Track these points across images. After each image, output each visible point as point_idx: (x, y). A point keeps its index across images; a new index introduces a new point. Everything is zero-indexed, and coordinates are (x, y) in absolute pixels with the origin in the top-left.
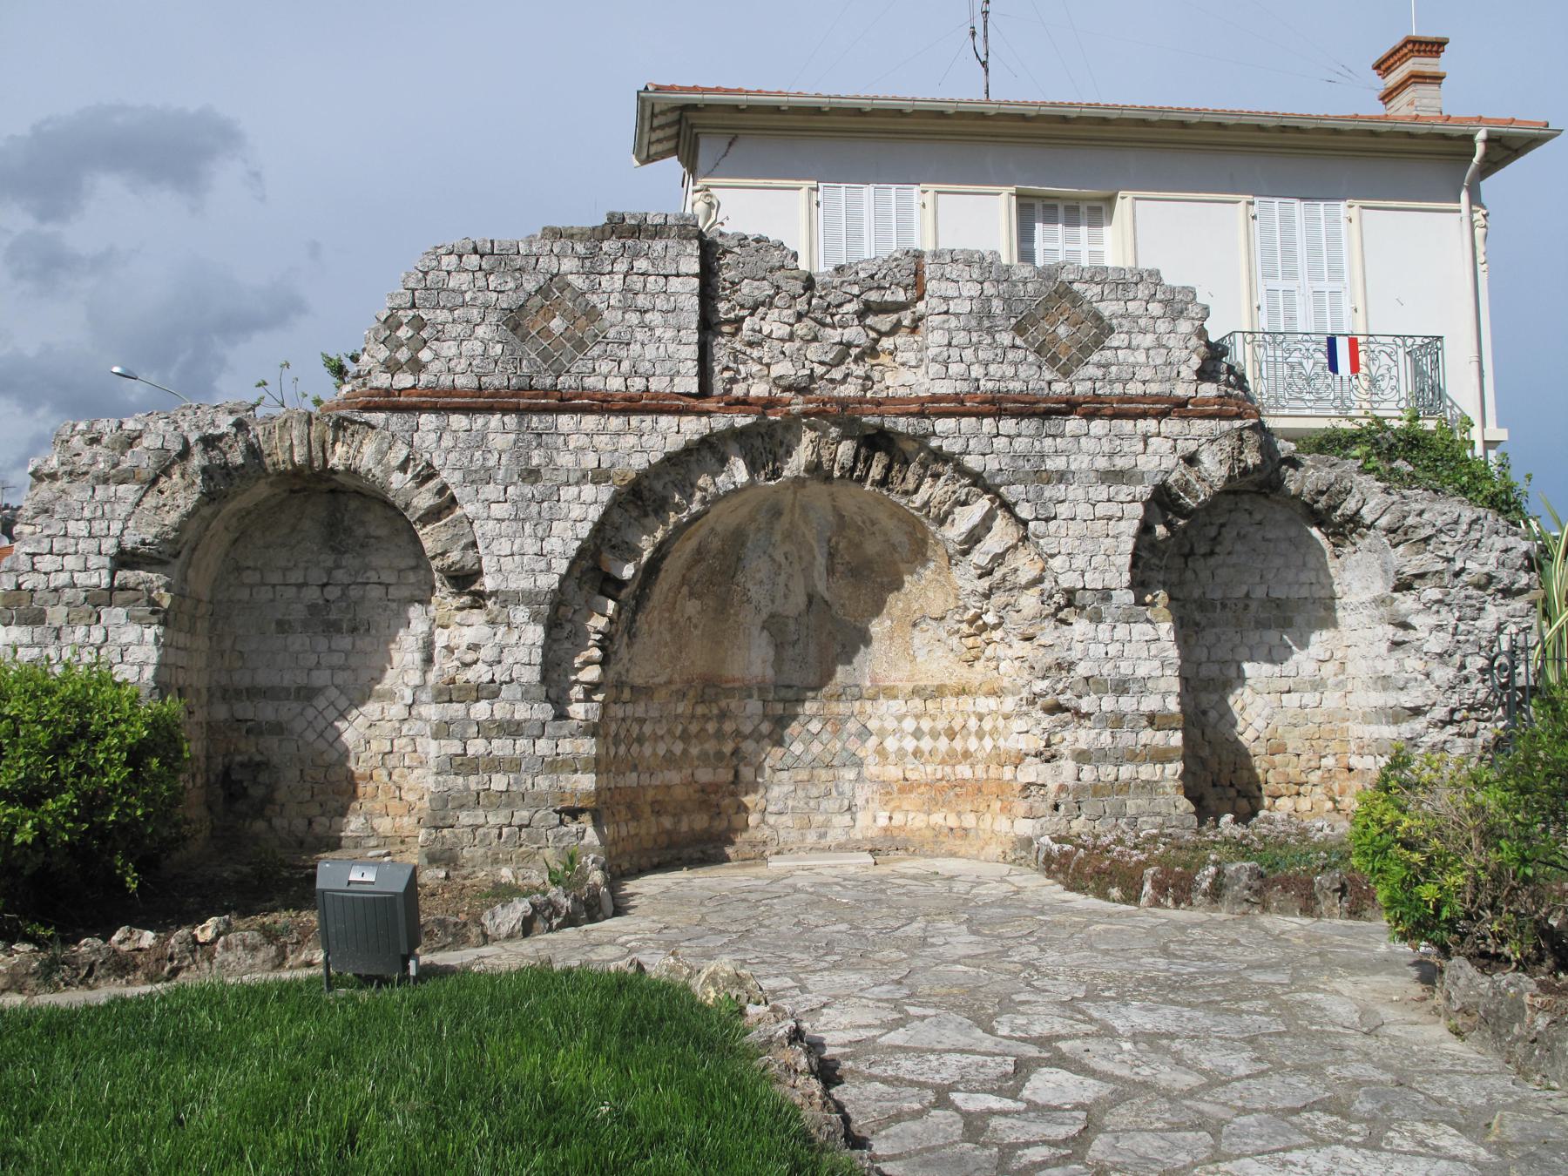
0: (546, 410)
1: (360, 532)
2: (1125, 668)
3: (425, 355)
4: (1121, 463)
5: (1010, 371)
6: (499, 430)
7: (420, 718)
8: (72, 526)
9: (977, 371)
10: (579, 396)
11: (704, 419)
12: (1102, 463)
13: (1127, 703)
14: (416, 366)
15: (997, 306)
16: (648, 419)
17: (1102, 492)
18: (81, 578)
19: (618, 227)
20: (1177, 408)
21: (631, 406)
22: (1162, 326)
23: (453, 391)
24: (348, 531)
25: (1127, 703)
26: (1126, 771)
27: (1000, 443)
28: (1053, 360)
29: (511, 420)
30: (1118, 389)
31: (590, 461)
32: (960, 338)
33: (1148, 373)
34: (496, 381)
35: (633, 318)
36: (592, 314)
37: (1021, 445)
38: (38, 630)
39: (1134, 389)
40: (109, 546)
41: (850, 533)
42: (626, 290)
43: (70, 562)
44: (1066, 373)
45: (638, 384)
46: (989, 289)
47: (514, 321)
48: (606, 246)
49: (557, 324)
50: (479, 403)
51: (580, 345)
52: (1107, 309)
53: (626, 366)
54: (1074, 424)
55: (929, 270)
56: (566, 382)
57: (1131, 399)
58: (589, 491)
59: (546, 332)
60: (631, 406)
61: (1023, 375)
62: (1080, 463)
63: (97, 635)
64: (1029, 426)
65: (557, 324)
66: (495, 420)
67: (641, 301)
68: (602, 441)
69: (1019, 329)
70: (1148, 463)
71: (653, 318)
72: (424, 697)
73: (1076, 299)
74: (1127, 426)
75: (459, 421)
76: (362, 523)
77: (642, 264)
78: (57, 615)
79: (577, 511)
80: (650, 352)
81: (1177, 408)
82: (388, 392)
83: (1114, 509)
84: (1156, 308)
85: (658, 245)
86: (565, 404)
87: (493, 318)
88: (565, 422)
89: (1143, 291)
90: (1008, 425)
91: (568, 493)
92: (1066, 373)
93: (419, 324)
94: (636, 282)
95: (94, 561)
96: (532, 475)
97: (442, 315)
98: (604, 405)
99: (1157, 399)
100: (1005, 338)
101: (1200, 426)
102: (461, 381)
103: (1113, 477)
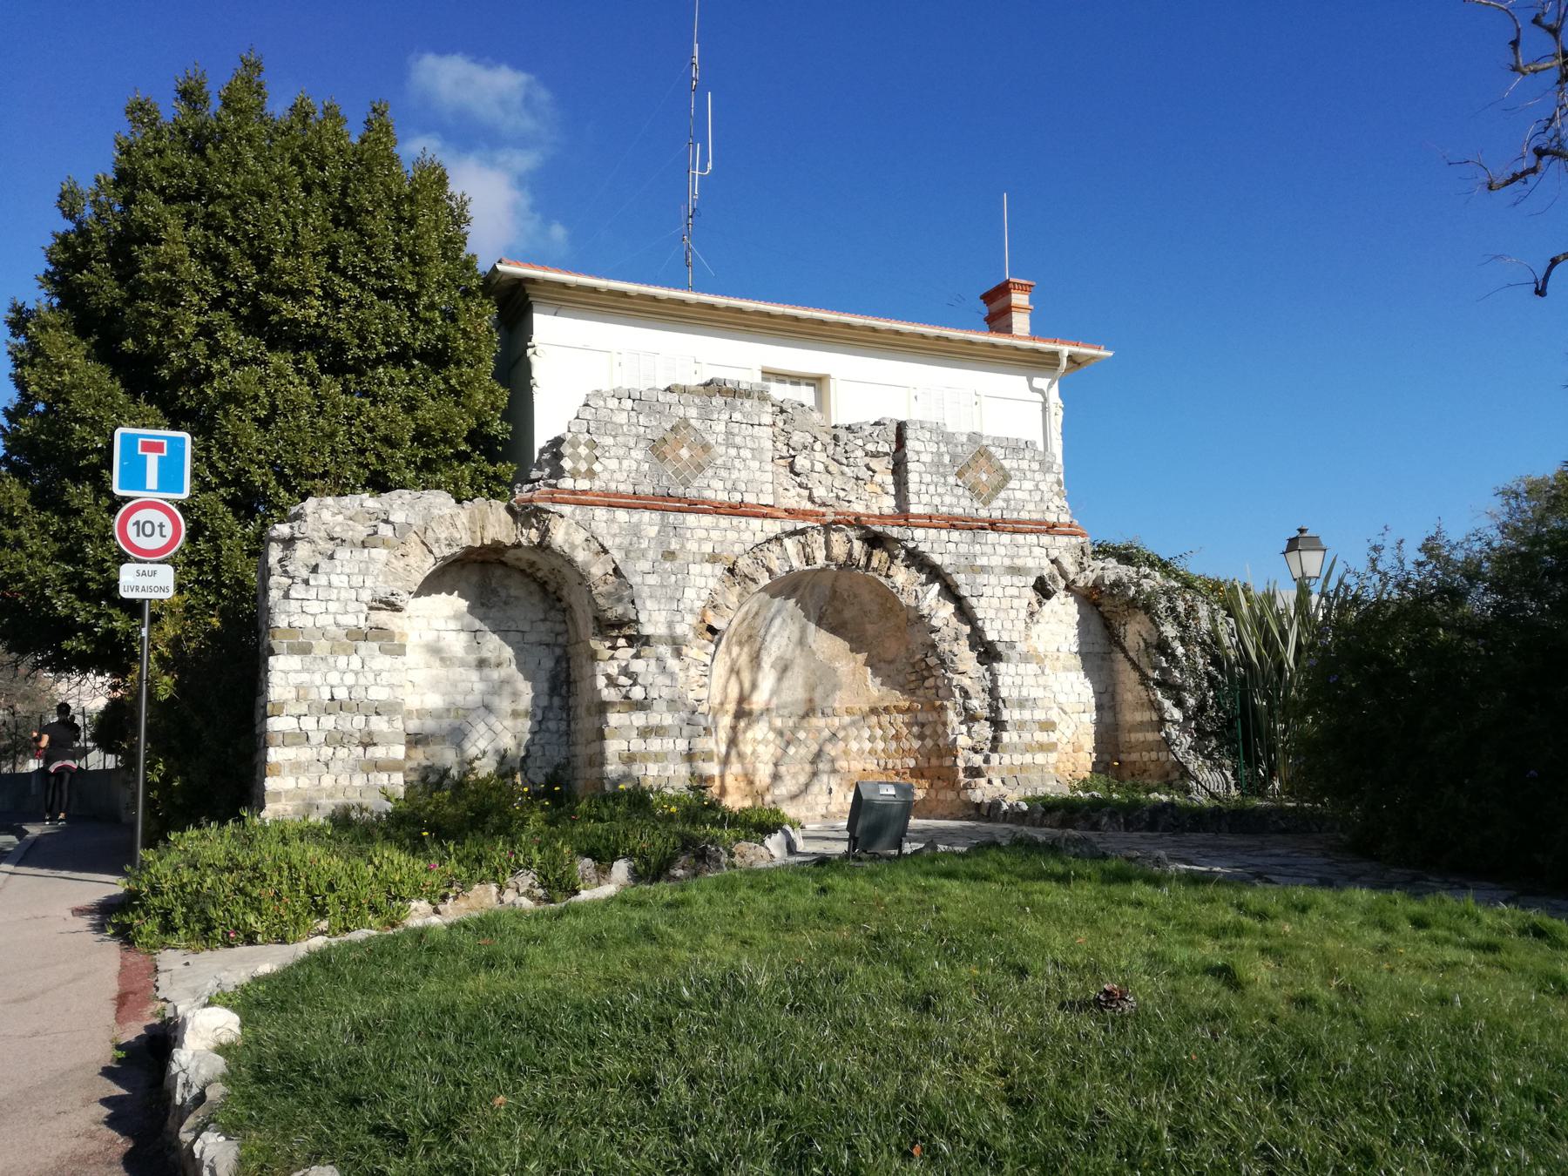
0: (679, 510)
1: (503, 593)
2: (1025, 693)
3: (597, 467)
4: (1019, 562)
5: (955, 501)
6: (649, 521)
7: (548, 730)
8: (334, 579)
9: (937, 500)
10: (703, 503)
11: (778, 522)
12: (1007, 562)
13: (1027, 715)
14: (591, 474)
15: (947, 459)
16: (743, 520)
17: (1006, 580)
18: (343, 620)
19: (713, 387)
20: (1051, 529)
21: (736, 510)
22: (1038, 476)
23: (617, 494)
24: (495, 592)
25: (1027, 715)
26: (1028, 758)
27: (951, 546)
28: (979, 495)
29: (656, 516)
30: (1015, 515)
31: (707, 548)
32: (927, 478)
33: (1031, 506)
34: (646, 489)
35: (733, 452)
36: (706, 447)
37: (963, 548)
38: (308, 658)
39: (1024, 516)
40: (366, 596)
41: (837, 603)
42: (729, 433)
43: (333, 607)
44: (986, 503)
45: (737, 497)
46: (943, 449)
47: (657, 449)
48: (714, 401)
49: (685, 453)
50: (634, 502)
51: (700, 468)
52: (1007, 464)
53: (729, 485)
54: (992, 536)
55: (910, 433)
56: (692, 493)
57: (1024, 522)
58: (708, 568)
59: (678, 459)
60: (736, 510)
61: (961, 505)
62: (995, 561)
63: (355, 662)
64: (967, 535)
65: (685, 453)
66: (646, 515)
67: (738, 440)
68: (715, 535)
69: (959, 475)
70: (1030, 563)
71: (746, 453)
72: (551, 715)
73: (990, 457)
74: (1019, 538)
75: (622, 515)
76: (506, 587)
77: (737, 416)
78: (321, 646)
79: (701, 582)
80: (744, 475)
81: (1051, 529)
82: (574, 492)
83: (1015, 591)
84: (1036, 466)
85: (747, 403)
86: (694, 506)
87: (642, 445)
88: (691, 519)
89: (1028, 454)
90: (955, 535)
91: (694, 569)
92: (986, 503)
93: (593, 445)
94: (735, 428)
95: (353, 606)
96: (670, 555)
97: (609, 441)
98: (717, 509)
99: (1039, 523)
100: (952, 480)
101: (1062, 541)
102: (622, 488)
103: (1015, 571)
